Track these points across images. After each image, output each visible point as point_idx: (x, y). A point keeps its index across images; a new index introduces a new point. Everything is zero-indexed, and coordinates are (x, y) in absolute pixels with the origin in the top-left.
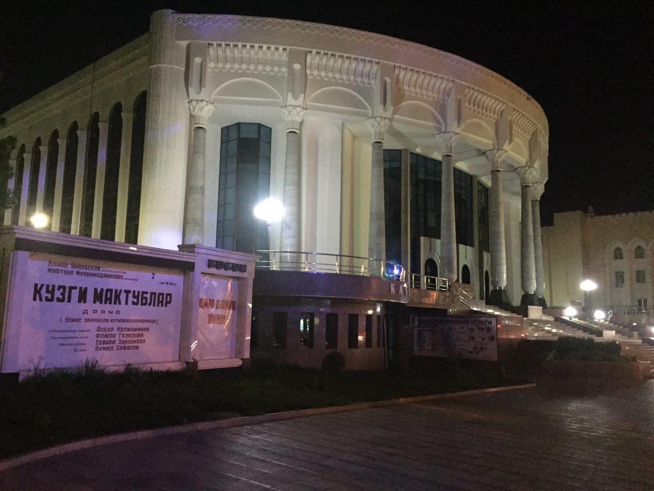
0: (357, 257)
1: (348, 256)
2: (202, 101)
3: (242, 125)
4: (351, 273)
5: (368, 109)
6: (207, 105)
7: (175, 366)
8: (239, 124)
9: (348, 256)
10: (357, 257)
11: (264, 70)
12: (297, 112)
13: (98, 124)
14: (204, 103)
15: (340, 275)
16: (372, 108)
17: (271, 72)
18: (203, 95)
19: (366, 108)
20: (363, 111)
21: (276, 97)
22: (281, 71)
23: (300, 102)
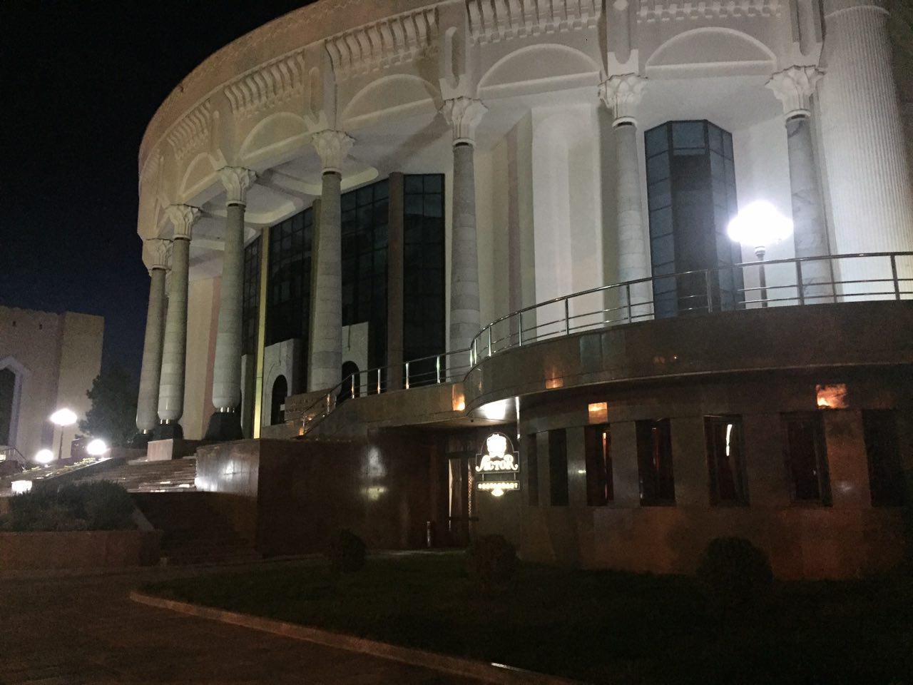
0: (889, 280)
1: (842, 282)
2: (460, 98)
3: (675, 127)
4: (831, 300)
5: (770, 58)
6: (470, 104)
7: (69, 314)
8: (669, 125)
9: (842, 282)
10: (889, 280)
11: (665, 14)
12: (630, 86)
13: (466, 407)
14: (465, 102)
15: (802, 307)
16: (777, 54)
17: (706, 14)
18: (463, 88)
19: (765, 57)
20: (761, 62)
21: (765, 57)
22: (667, 13)
23: (632, 65)
